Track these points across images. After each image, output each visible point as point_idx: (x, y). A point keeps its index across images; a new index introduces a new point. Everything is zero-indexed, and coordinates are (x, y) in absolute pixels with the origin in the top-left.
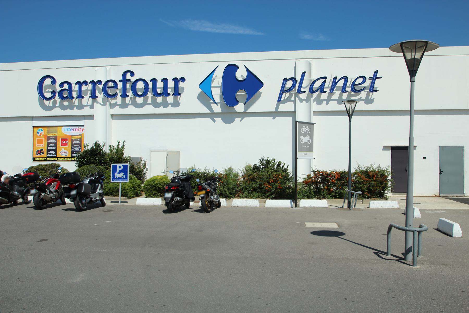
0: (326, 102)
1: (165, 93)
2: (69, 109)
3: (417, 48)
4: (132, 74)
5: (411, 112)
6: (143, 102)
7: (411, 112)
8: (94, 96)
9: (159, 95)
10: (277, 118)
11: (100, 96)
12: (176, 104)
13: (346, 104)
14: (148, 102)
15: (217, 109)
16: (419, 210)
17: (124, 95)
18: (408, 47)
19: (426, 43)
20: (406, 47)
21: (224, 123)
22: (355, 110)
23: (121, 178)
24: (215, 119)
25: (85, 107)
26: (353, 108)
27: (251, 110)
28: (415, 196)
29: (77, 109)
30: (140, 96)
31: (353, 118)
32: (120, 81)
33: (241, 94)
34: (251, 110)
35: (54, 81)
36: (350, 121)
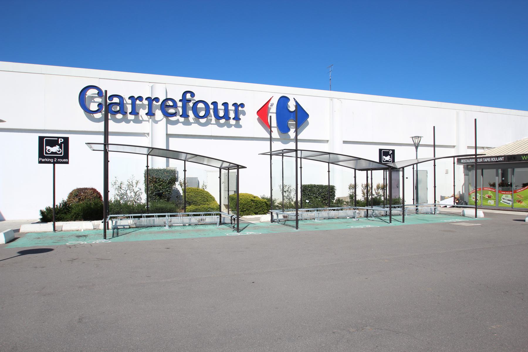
1: (226, 117)
2: (124, 122)
4: (193, 94)
5: (434, 146)
6: (205, 122)
7: (434, 146)
8: (150, 114)
9: (222, 118)
11: (159, 114)
12: (238, 126)
14: (212, 123)
17: (185, 115)
21: (282, 144)
22: (420, 144)
23: (56, 152)
25: (192, 124)
28: (110, 150)
30: (202, 117)
31: (419, 148)
32: (180, 101)
33: (291, 123)
36: (417, 151)
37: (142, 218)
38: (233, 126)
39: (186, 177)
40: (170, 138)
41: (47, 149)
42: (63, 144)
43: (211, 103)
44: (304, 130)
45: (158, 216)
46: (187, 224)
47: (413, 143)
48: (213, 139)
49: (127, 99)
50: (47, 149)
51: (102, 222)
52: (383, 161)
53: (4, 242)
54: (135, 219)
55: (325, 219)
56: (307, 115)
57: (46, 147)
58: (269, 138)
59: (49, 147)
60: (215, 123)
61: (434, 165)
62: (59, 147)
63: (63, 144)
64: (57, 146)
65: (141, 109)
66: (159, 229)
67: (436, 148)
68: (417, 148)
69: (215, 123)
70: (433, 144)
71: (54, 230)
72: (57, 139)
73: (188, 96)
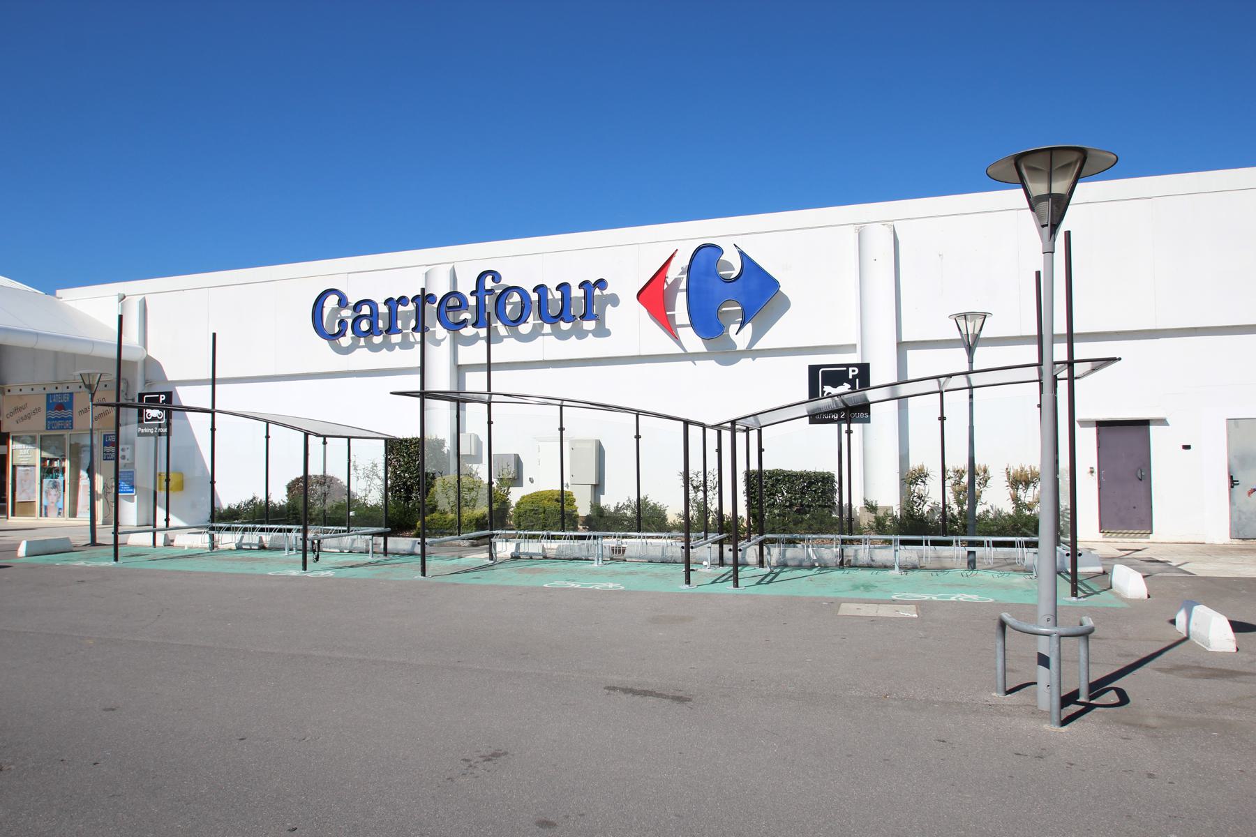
0: (459, 346)
3: (1054, 169)
4: (496, 276)
10: (757, 359)
12: (602, 332)
13: (958, 321)
15: (692, 341)
16: (1228, 623)
18: (1038, 167)
19: (1083, 153)
20: (1029, 168)
21: (717, 364)
22: (982, 336)
24: (696, 362)
25: (505, 339)
26: (976, 332)
27: (762, 344)
28: (149, 533)
29: (401, 348)
32: (472, 293)
34: (762, 344)
35: (343, 302)
37: (922, 545)
38: (590, 335)
39: (493, 453)
40: (908, 351)
41: (825, 392)
42: (857, 380)
43: (580, 282)
44: (779, 321)
45: (900, 540)
46: (346, 549)
47: (959, 337)
48: (551, 369)
49: (554, 290)
50: (825, 392)
51: (730, 550)
52: (147, 420)
53: (24, 555)
54: (906, 547)
55: (651, 562)
56: (775, 284)
57: (823, 388)
58: (1063, 335)
59: (830, 387)
60: (364, 344)
61: (210, 427)
62: (849, 386)
63: (857, 380)
64: (845, 384)
65: (609, 305)
66: (996, 576)
67: (492, 372)
68: (970, 350)
69: (550, 332)
70: (485, 361)
71: (213, 546)
72: (845, 369)
73: (489, 283)
